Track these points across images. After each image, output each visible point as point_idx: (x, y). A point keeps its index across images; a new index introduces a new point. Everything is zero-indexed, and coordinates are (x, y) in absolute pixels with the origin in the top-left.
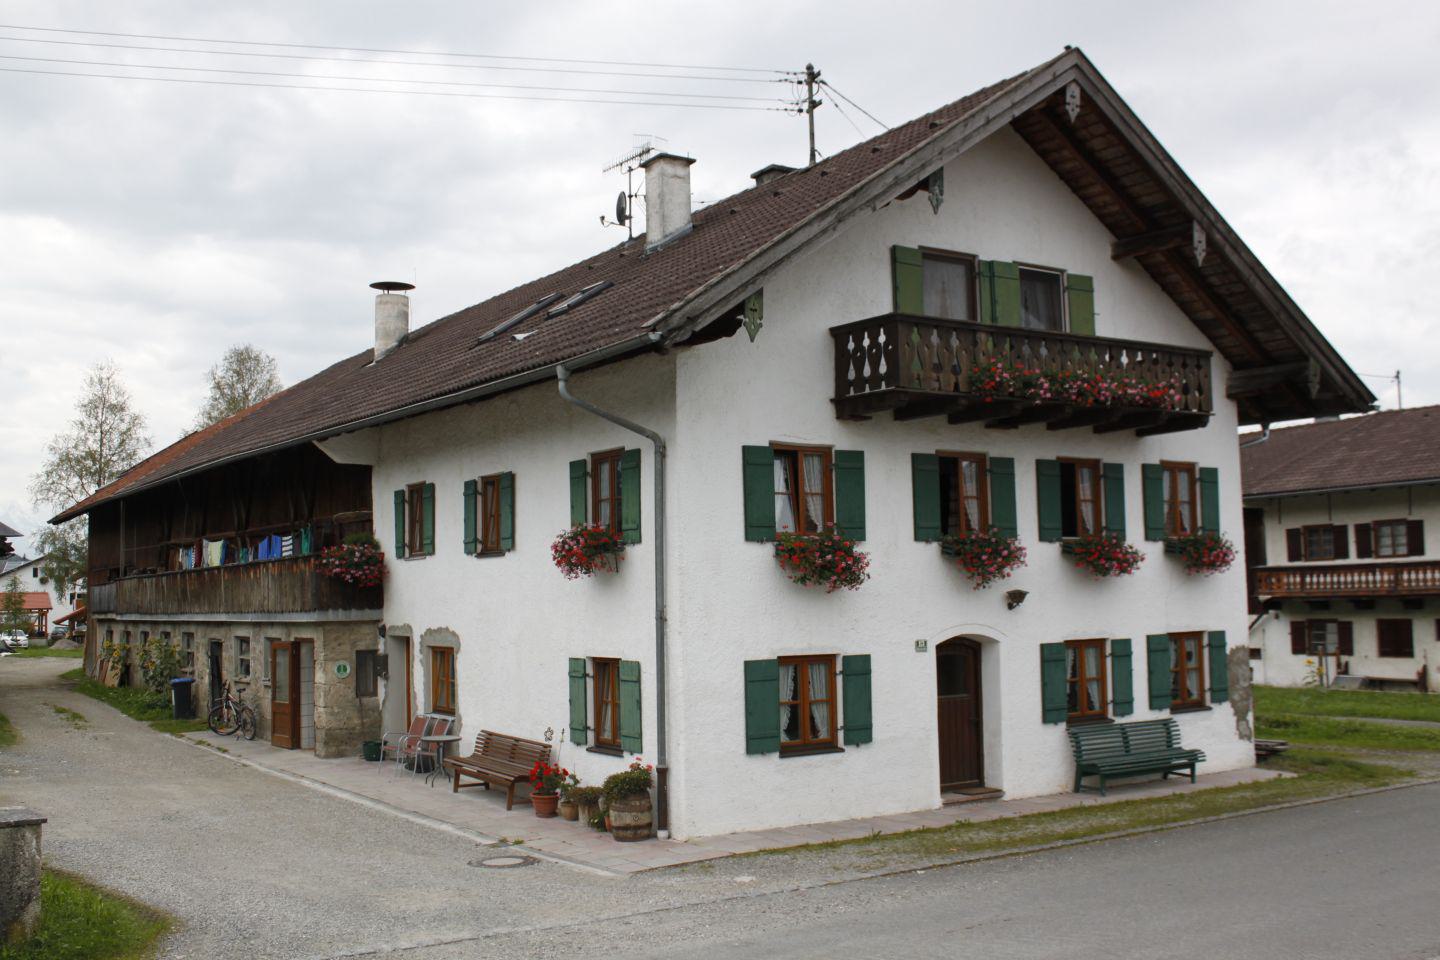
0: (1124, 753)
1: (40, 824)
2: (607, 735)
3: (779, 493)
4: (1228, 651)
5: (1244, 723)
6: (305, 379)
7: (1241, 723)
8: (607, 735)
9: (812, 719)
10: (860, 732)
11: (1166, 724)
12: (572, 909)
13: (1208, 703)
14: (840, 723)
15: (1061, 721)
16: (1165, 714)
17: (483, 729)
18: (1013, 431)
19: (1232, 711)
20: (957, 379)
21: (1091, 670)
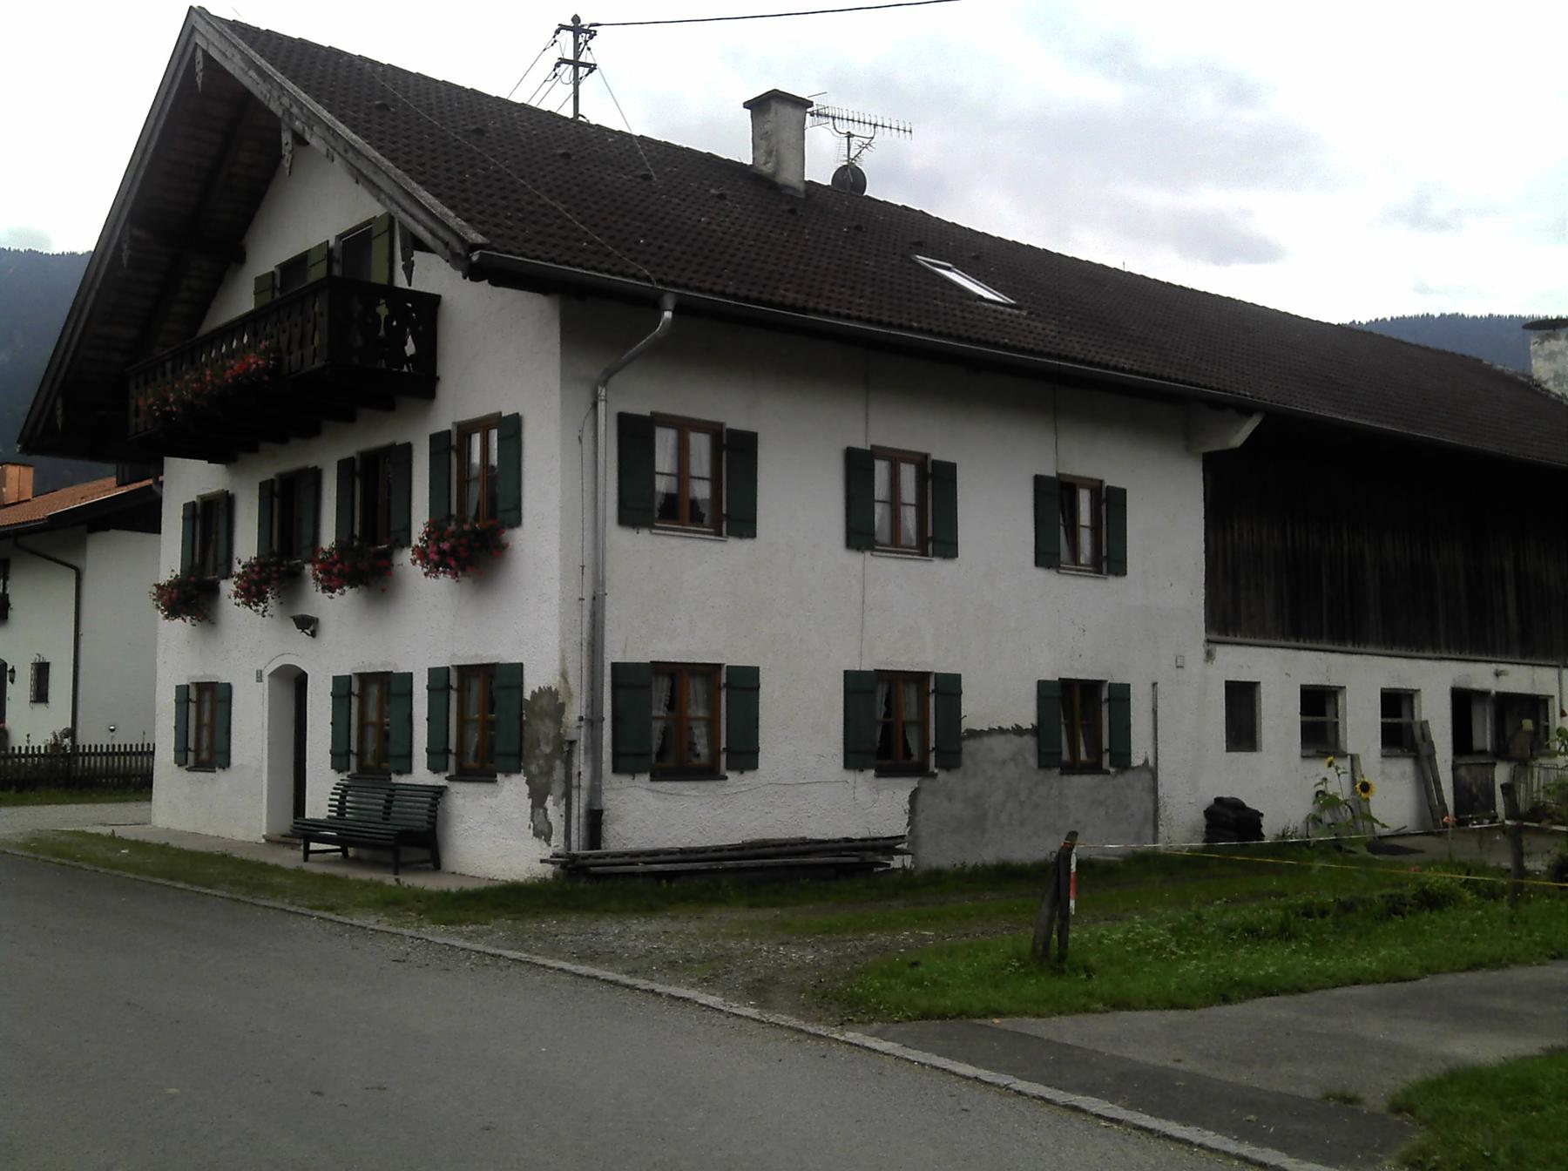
0: (381, 820)
1: (195, 767)
2: (204, 755)
3: (878, 501)
4: (527, 695)
5: (541, 811)
6: (759, 484)
7: (537, 810)
8: (204, 755)
9: (906, 742)
10: (745, 756)
11: (439, 792)
12: (673, 825)
13: (933, 768)
14: (932, 744)
15: (869, 767)
16: (439, 780)
17: (1017, 723)
18: (247, 257)
19: (526, 789)
20: (318, 135)
21: (909, 711)
